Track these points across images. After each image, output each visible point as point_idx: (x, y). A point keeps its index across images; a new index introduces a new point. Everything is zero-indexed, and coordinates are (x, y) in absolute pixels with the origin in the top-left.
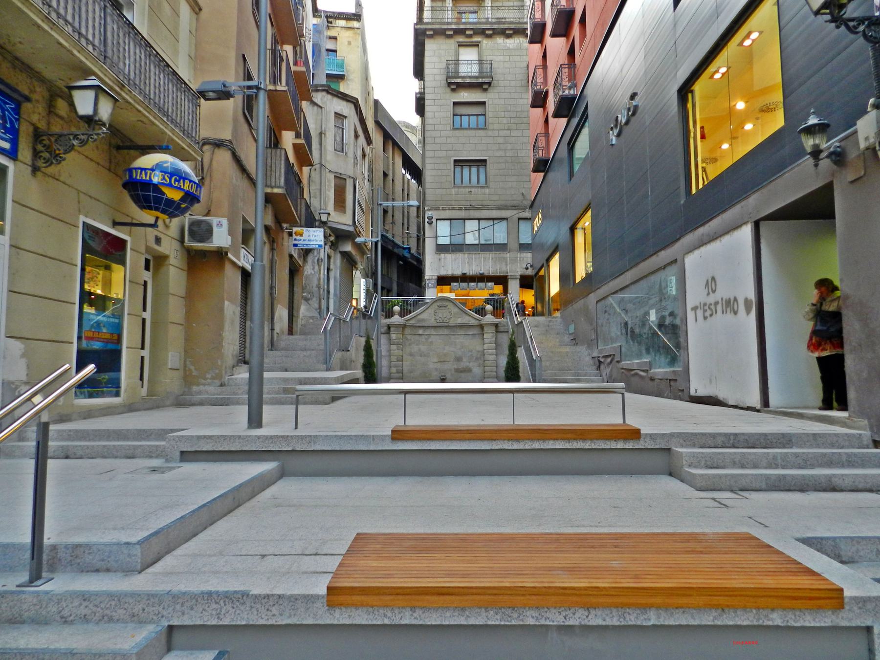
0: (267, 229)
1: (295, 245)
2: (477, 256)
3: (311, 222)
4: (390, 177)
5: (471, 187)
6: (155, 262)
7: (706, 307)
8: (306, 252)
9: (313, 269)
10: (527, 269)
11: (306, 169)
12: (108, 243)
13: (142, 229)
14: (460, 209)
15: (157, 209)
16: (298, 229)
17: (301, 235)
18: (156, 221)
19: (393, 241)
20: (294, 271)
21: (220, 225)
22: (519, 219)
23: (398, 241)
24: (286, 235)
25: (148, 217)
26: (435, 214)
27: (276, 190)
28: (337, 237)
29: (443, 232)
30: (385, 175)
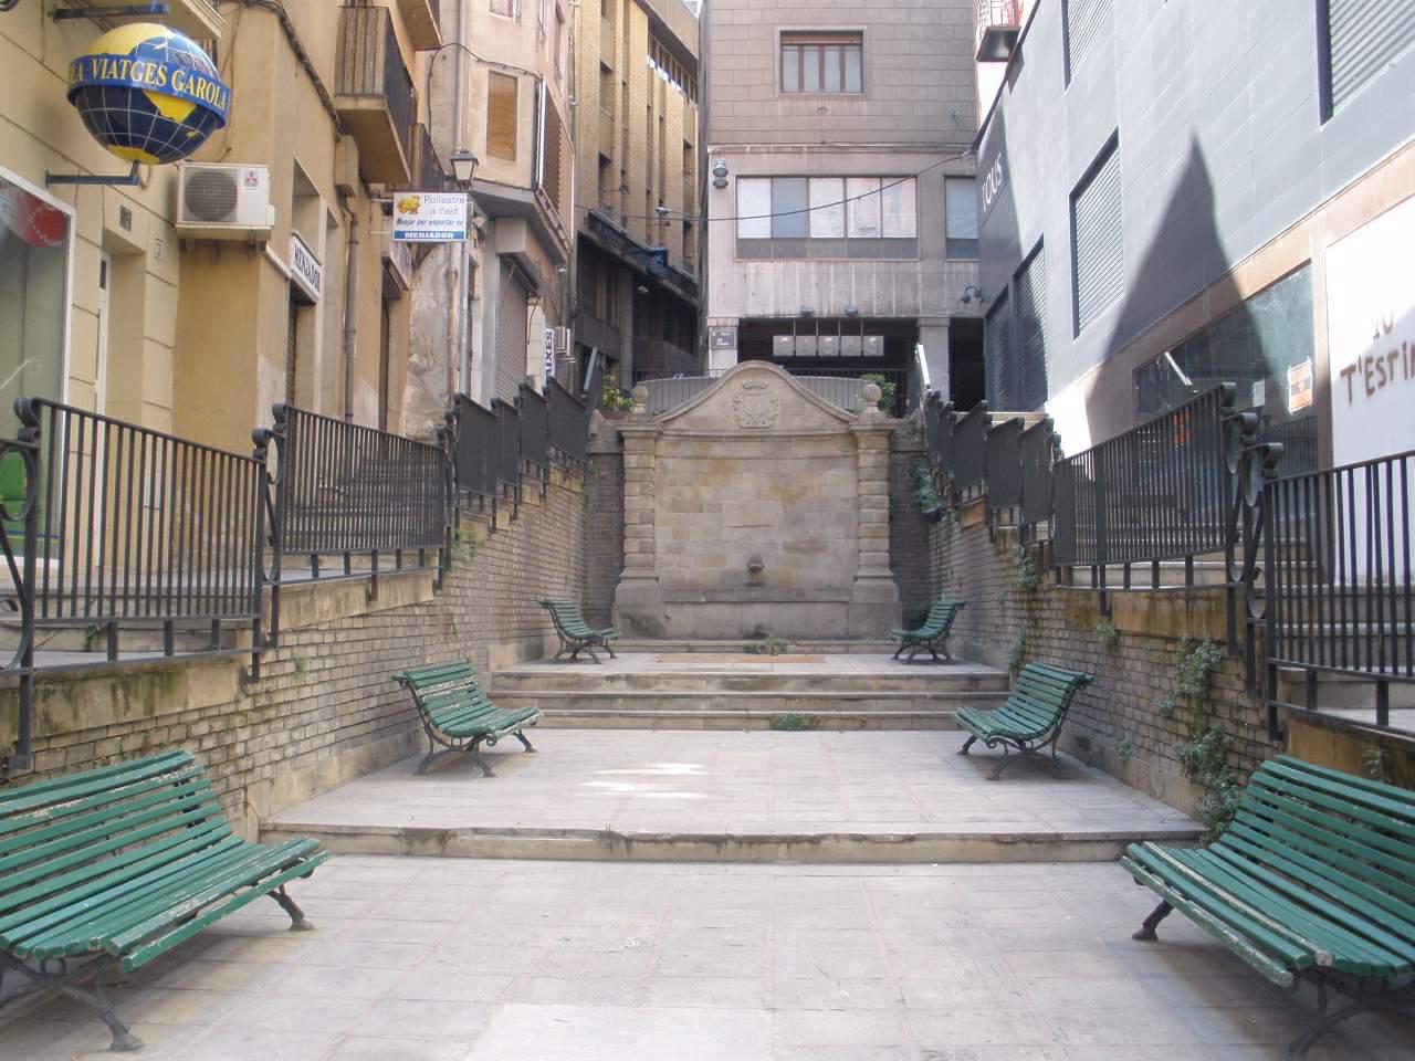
0: (342, 193)
1: (400, 235)
2: (841, 268)
3: (437, 179)
4: (619, 78)
5: (823, 98)
6: (119, 258)
7: (1372, 367)
8: (422, 252)
9: (435, 297)
10: (966, 300)
11: (422, 56)
12: (37, 220)
13: (97, 187)
14: (798, 151)
15: (137, 143)
16: (408, 196)
17: (414, 211)
18: (135, 170)
19: (623, 236)
20: (392, 293)
21: (252, 180)
22: (947, 177)
23: (636, 233)
24: (377, 211)
25: (114, 162)
26: (734, 165)
27: (365, 104)
28: (494, 212)
29: (750, 208)
30: (606, 71)
